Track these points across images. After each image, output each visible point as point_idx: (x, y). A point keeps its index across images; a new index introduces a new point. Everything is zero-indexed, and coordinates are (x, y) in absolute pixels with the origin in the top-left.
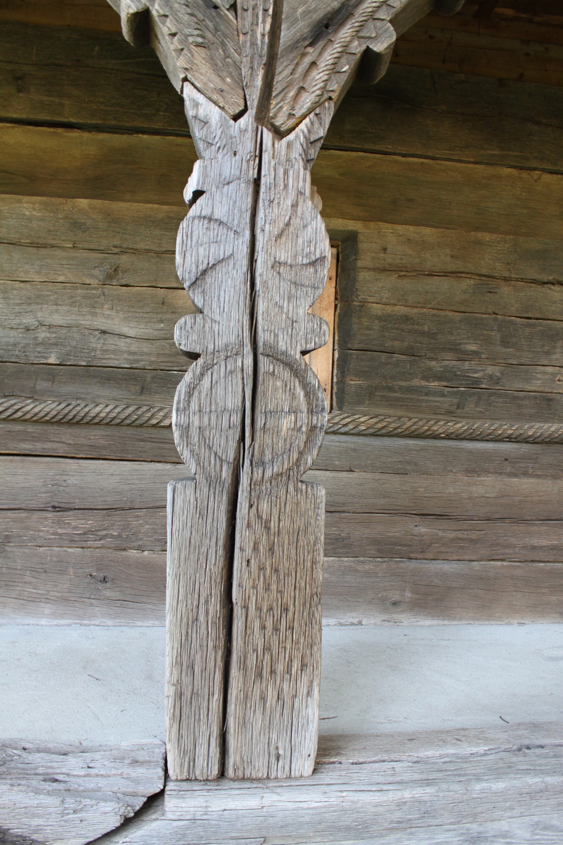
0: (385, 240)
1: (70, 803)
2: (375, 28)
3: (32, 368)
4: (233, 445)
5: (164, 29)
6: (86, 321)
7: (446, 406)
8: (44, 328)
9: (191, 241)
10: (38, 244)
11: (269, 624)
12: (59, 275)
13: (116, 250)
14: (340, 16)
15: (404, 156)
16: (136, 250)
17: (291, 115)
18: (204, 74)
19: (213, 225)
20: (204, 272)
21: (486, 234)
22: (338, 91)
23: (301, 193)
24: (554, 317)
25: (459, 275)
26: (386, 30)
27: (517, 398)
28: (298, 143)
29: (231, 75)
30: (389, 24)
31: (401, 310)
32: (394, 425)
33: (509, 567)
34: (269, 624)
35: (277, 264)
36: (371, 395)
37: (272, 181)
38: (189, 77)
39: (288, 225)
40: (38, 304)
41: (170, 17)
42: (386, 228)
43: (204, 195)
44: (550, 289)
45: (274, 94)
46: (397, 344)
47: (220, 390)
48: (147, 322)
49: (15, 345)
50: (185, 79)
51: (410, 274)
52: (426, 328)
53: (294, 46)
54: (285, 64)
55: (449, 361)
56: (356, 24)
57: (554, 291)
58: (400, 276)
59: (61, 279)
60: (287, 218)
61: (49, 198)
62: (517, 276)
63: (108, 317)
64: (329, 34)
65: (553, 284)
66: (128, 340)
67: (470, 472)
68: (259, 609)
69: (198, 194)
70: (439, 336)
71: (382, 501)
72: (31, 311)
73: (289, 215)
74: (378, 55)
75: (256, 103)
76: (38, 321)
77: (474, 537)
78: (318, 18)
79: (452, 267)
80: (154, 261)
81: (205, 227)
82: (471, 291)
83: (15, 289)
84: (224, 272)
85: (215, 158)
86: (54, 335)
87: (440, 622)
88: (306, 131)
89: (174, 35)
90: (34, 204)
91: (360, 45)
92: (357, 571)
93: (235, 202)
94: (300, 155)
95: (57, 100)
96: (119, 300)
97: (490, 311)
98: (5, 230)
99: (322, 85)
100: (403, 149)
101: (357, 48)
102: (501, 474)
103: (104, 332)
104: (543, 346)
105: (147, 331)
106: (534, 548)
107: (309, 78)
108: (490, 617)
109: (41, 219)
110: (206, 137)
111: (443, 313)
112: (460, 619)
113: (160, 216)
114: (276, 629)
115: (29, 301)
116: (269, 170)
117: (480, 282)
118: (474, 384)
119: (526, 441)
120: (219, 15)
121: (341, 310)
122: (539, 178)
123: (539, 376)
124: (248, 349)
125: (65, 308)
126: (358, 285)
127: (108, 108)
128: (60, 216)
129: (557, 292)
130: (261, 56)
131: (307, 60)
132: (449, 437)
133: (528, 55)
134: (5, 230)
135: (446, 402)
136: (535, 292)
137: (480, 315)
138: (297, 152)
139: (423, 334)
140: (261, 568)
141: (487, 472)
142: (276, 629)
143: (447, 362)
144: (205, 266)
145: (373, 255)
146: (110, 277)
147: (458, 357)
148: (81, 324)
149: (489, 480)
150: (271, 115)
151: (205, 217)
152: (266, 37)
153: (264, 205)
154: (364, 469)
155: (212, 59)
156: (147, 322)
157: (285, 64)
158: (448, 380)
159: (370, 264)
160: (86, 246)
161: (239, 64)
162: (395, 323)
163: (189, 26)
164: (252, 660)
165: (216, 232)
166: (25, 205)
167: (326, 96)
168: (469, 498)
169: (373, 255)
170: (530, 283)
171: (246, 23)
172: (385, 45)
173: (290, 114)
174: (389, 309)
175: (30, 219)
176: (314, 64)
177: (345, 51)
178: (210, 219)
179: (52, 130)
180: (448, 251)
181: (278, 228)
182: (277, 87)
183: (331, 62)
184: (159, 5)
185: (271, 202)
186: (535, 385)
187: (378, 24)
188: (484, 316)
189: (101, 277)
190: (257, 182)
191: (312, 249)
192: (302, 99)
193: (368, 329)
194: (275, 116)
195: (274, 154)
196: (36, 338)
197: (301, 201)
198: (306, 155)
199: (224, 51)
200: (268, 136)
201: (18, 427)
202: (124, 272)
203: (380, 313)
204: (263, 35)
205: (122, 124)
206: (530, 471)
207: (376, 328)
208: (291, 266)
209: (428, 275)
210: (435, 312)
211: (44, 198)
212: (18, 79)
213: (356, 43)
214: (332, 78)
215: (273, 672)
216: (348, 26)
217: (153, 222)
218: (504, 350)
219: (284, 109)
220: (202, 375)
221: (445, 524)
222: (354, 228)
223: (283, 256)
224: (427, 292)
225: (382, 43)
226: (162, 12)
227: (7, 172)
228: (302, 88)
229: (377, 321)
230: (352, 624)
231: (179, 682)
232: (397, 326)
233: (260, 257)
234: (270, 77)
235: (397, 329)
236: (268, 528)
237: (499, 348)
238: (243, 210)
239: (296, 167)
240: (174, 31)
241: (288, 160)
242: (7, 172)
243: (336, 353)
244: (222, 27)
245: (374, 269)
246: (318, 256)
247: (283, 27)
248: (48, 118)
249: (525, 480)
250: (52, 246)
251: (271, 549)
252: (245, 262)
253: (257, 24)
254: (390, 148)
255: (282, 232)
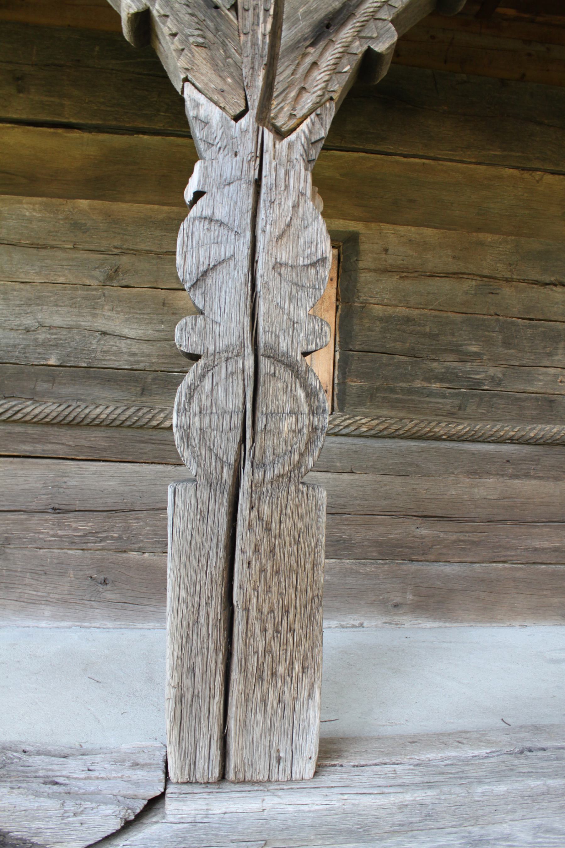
0: (386, 241)
1: (71, 806)
2: (377, 28)
3: (32, 369)
4: (234, 446)
5: (164, 29)
6: (86, 322)
7: (448, 407)
8: (44, 329)
9: (192, 241)
10: (38, 244)
11: (270, 626)
12: (59, 276)
13: (116, 251)
14: (342, 16)
15: (405, 156)
16: (137, 251)
17: (292, 116)
18: (205, 74)
19: (214, 226)
20: (205, 273)
21: (488, 235)
22: (339, 92)
23: (302, 194)
24: (556, 318)
25: (461, 276)
26: (388, 30)
27: (519, 399)
28: (299, 144)
29: (232, 76)
30: (390, 24)
31: (402, 311)
32: (395, 427)
33: (510, 569)
34: (270, 626)
35: (278, 265)
36: (372, 397)
37: (273, 182)
38: (190, 77)
39: (289, 225)
40: (38, 305)
41: (171, 17)
42: (388, 228)
43: (205, 195)
44: (552, 290)
45: (275, 94)
46: (398, 345)
47: (220, 391)
48: (147, 323)
49: (15, 346)
50: (186, 80)
51: (412, 275)
52: (428, 329)
53: (295, 46)
54: (286, 64)
55: (450, 363)
56: (358, 24)
57: (556, 292)
58: (401, 277)
59: (61, 280)
60: (288, 219)
61: (49, 199)
62: (519, 277)
63: (109, 318)
64: (330, 34)
65: (555, 285)
66: (129, 341)
67: (472, 473)
68: (260, 611)
69: (198, 195)
70: (441, 338)
71: (384, 503)
72: (31, 312)
73: (290, 216)
74: (379, 56)
75: (256, 103)
76: (39, 322)
77: (475, 539)
78: (319, 18)
79: (453, 268)
80: (154, 261)
81: (205, 228)
82: (473, 292)
83: (15, 290)
84: (225, 273)
85: (216, 158)
86: (54, 337)
87: (442, 624)
88: (307, 131)
89: (174, 35)
90: (34, 204)
91: (361, 45)
92: (358, 573)
93: (236, 203)
94: (301, 155)
95: (57, 100)
96: (120, 301)
97: (492, 312)
98: (5, 231)
99: (323, 85)
100: (404, 150)
101: (359, 48)
102: (502, 475)
103: (104, 333)
104: (545, 347)
105: (147, 332)
106: (536, 550)
107: (310, 78)
108: (492, 619)
109: (42, 220)
110: (207, 138)
111: (444, 314)
112: (462, 622)
113: (161, 216)
114: (277, 631)
115: (29, 302)
116: (270, 171)
117: (481, 283)
118: (476, 385)
119: (528, 442)
120: (220, 15)
121: (342, 311)
122: (541, 179)
123: (541, 377)
124: (249, 350)
125: (66, 309)
126: (359, 286)
127: (109, 109)
128: (60, 217)
129: (559, 293)
130: (262, 57)
131: (308, 60)
132: (450, 439)
133: (530, 55)
134: (5, 231)
135: (448, 404)
136: (537, 293)
137: (482, 316)
138: (298, 152)
139: (424, 335)
140: (262, 570)
141: (488, 473)
142: (277, 631)
143: (448, 364)
144: (205, 267)
145: (375, 255)
146: (110, 278)
147: (459, 359)
148: (82, 326)
149: (490, 481)
150: (272, 115)
151: (205, 218)
152: (267, 37)
153: (265, 206)
154: (366, 470)
155: (213, 59)
156: (147, 323)
157: (286, 64)
158: (449, 381)
159: (372, 265)
160: (87, 247)
161: (239, 64)
162: (396, 324)
163: (190, 26)
164: (253, 663)
165: (217, 233)
166: (25, 206)
167: (327, 97)
168: (471, 500)
169: (375, 255)
170: (532, 284)
171: (247, 23)
172: (387, 45)
173: (291, 115)
174: (390, 310)
175: (30, 220)
176: (315, 64)
177: (346, 51)
178: (211, 220)
179: (52, 130)
180: (449, 252)
181: (279, 228)
182: (278, 87)
183: (332, 62)
184: (160, 5)
185: (272, 202)
186: (537, 386)
187: (380, 24)
188: (486, 317)
189: (101, 278)
190: (258, 183)
191: (314, 249)
192: (303, 99)
193: (370, 330)
194: (276, 116)
195: (275, 155)
196: (36, 340)
197: (302, 202)
198: (307, 156)
199: (224, 51)
200: (269, 136)
201: (19, 429)
202: (125, 273)
203: (381, 314)
204: (264, 35)
205: (122, 124)
206: (532, 473)
207: (377, 329)
208: (292, 267)
209: (430, 276)
210: (437, 313)
211: (44, 199)
212: (19, 79)
213: (357, 43)
214: (334, 78)
215: (274, 674)
216: (349, 26)
217: (154, 223)
218: (506, 351)
219: (285, 109)
220: (203, 376)
221: (446, 526)
222: (355, 229)
223: (284, 256)
224: (429, 293)
225: (383, 43)
226: (162, 13)
227: (7, 173)
228: (303, 89)
229: (378, 323)
230: (354, 626)
231: (180, 685)
232: (398, 327)
233: (261, 258)
234: (271, 77)
235: (399, 330)
236: (269, 530)
237: (501, 349)
238: (244, 211)
239: (297, 167)
240: (174, 31)
241: (289, 161)
242: (7, 173)
243: (337, 354)
244: (223, 27)
245: (375, 270)
246: (319, 257)
247: (284, 27)
248: (49, 119)
249: (527, 482)
250: (52, 247)
251: (272, 551)
252: (246, 263)
253: (258, 25)
254: (391, 148)
255: (283, 232)
